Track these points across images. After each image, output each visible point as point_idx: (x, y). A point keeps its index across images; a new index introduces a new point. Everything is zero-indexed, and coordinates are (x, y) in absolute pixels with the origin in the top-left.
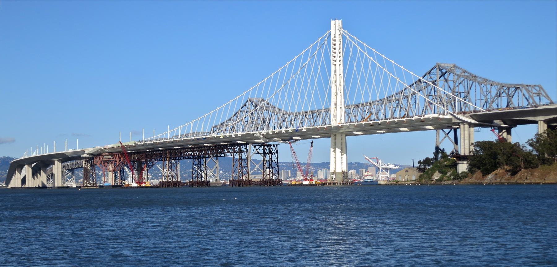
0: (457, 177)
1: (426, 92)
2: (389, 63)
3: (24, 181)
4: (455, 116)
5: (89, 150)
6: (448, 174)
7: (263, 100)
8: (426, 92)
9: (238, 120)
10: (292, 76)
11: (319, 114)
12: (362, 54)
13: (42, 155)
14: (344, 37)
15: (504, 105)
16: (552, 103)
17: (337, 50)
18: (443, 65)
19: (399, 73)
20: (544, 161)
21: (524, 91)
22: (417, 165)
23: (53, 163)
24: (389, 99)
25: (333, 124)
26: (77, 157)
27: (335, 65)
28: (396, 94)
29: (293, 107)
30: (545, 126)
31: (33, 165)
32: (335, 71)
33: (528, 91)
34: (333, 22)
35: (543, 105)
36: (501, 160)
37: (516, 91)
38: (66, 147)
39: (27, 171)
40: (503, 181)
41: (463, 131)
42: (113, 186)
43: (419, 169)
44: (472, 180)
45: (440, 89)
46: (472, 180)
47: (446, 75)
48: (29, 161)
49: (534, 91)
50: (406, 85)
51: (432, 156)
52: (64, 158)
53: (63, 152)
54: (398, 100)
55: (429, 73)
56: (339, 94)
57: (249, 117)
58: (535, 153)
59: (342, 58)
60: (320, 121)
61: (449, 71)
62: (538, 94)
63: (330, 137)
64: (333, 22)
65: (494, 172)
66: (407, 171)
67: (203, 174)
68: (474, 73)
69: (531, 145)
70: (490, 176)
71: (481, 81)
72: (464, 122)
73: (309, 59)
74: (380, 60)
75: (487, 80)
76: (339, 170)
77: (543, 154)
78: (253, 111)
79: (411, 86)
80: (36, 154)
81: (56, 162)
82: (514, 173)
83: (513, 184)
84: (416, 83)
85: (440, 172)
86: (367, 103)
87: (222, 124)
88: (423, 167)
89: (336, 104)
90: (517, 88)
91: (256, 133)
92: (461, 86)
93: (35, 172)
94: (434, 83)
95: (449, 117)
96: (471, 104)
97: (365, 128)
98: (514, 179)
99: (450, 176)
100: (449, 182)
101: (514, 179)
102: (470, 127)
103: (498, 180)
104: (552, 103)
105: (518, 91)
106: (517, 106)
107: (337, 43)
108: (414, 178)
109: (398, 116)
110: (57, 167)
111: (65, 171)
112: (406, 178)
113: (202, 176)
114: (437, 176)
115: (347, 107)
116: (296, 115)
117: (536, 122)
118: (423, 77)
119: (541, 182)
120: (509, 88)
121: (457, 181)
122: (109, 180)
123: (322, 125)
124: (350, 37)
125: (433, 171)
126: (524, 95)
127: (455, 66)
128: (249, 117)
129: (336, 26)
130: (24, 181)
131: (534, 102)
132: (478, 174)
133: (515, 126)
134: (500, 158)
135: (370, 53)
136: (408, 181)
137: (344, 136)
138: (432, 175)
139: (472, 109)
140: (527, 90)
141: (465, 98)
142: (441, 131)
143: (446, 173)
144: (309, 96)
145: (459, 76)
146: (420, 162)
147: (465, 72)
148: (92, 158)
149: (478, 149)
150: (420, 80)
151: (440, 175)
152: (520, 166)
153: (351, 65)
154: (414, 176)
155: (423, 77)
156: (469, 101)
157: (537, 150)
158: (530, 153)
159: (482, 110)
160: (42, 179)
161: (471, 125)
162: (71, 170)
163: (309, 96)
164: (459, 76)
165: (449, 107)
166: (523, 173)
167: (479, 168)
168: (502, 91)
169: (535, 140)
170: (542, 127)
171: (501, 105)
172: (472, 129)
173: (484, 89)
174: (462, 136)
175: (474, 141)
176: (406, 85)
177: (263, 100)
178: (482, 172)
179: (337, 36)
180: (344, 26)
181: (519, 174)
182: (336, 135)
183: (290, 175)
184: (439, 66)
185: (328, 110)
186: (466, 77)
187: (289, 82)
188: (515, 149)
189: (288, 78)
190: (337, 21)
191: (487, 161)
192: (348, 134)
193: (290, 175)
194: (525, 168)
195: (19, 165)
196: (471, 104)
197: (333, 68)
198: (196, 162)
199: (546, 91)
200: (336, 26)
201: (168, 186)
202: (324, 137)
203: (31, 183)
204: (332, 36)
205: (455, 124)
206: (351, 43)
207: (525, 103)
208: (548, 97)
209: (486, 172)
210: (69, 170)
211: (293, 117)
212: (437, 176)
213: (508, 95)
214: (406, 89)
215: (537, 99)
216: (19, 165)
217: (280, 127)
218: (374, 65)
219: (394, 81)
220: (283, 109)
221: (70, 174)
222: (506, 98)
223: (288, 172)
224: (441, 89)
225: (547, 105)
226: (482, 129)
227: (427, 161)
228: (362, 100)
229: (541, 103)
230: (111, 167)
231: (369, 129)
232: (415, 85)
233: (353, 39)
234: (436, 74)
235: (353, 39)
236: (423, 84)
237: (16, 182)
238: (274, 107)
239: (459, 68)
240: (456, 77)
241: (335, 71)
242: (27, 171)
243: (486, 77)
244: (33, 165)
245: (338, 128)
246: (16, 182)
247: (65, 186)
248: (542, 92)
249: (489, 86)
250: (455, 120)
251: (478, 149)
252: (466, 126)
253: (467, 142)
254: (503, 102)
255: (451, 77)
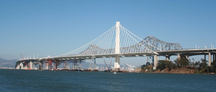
0: (153, 71)
1: (144, 44)
2: (134, 36)
3: (20, 67)
4: (152, 52)
5: (41, 59)
6: (150, 70)
7: (95, 45)
8: (144, 44)
9: (87, 51)
10: (104, 38)
11: (112, 50)
12: (125, 32)
13: (26, 59)
14: (120, 27)
15: (168, 49)
16: (182, 49)
17: (118, 31)
18: (150, 36)
19: (136, 39)
20: (179, 67)
21: (174, 45)
22: (141, 67)
23: (30, 62)
24: (133, 46)
25: (116, 54)
26: (37, 60)
27: (117, 35)
28: (135, 45)
29: (104, 47)
30: (180, 56)
31: (23, 63)
32: (117, 37)
33: (175, 45)
34: (117, 22)
35: (179, 50)
36: (166, 66)
37: (171, 45)
38: (34, 57)
39: (21, 64)
40: (166, 73)
41: (155, 57)
42: (48, 70)
43: (142, 68)
44: (156, 72)
45: (149, 44)
46: (156, 72)
47: (151, 40)
48: (22, 61)
49: (177, 45)
50: (138, 42)
51: (145, 64)
52: (33, 61)
53: (33, 59)
54: (136, 47)
55: (146, 39)
56: (118, 45)
57: (91, 50)
58: (176, 64)
59: (119, 33)
60: (112, 52)
61: (152, 39)
62: (178, 46)
63: (115, 57)
64: (117, 22)
65: (164, 70)
66: (138, 69)
67: (67, 67)
68: (159, 39)
69: (175, 62)
70: (162, 71)
71: (161, 42)
72: (155, 54)
73: (109, 33)
74: (131, 34)
75: (163, 42)
76: (117, 68)
77: (179, 65)
78: (92, 48)
79: (140, 43)
80: (25, 59)
81: (31, 62)
82: (170, 70)
83: (169, 73)
84: (141, 42)
85: (148, 69)
86: (129, 47)
87: (82, 52)
88: (142, 67)
89: (117, 47)
90: (172, 44)
91: (93, 55)
92: (155, 43)
93: (24, 65)
94: (147, 42)
95: (151, 52)
96: (158, 49)
97: (140, 54)
98: (170, 72)
99: (151, 70)
100: (150, 72)
101: (170, 72)
102: (157, 56)
103: (165, 72)
104: (182, 49)
105: (172, 45)
106: (172, 50)
107: (118, 29)
108: (140, 71)
109: (141, 51)
110: (31, 63)
111: (34, 65)
112: (138, 70)
113: (66, 68)
114: (147, 70)
115: (120, 48)
116: (105, 50)
117: (177, 55)
118: (144, 40)
119: (178, 73)
120: (169, 44)
121: (152, 72)
122: (47, 68)
123: (89, 55)
124: (122, 27)
125: (146, 68)
126: (174, 46)
127: (153, 37)
128: (91, 50)
129: (118, 24)
130: (20, 67)
131: (177, 49)
132: (159, 70)
133: (171, 56)
134: (166, 66)
135: (128, 32)
136: (138, 71)
137: (119, 57)
138: (145, 70)
139: (158, 50)
140: (175, 45)
141: (156, 47)
142: (148, 57)
143: (149, 70)
144: (109, 44)
145: (155, 40)
146: (142, 66)
147: (156, 39)
148: (42, 61)
149: (159, 62)
150: (143, 41)
151: (148, 70)
152: (172, 68)
153: (122, 35)
154: (140, 70)
155: (144, 40)
156: (157, 48)
157: (177, 63)
158: (175, 64)
159: (161, 51)
160: (26, 68)
161: (157, 55)
162: (36, 64)
163: (109, 44)
164: (155, 40)
165: (151, 49)
166: (172, 70)
167: (159, 68)
168: (167, 45)
169: (176, 60)
170: (178, 56)
171: (166, 50)
172: (158, 57)
173: (162, 44)
174: (155, 58)
175: (158, 60)
176: (138, 42)
177: (95, 45)
178: (160, 69)
179: (118, 26)
180: (120, 24)
181: (171, 70)
182: (116, 57)
183: (104, 68)
184: (149, 37)
185: (114, 49)
186: (157, 40)
187: (103, 40)
188: (170, 63)
189: (103, 39)
190: (118, 22)
191: (162, 66)
192: (121, 57)
193: (104, 68)
194: (173, 69)
195: (19, 63)
196: (158, 49)
197: (116, 36)
198: (74, 63)
199: (181, 45)
200: (118, 24)
201: (74, 71)
202: (107, 57)
203: (22, 68)
204: (117, 27)
205: (153, 55)
206: (122, 29)
207: (174, 49)
208: (181, 47)
209: (161, 70)
210: (35, 64)
211: (104, 51)
212: (147, 70)
213: (169, 46)
214: (138, 44)
215: (178, 48)
216: (19, 63)
217: (100, 54)
218: (129, 36)
219: (135, 41)
220: (101, 48)
221: (35, 65)
222: (169, 47)
223: (103, 67)
224: (149, 44)
225: (181, 50)
226: (160, 56)
227: (144, 66)
228: (125, 46)
229: (179, 49)
230: (48, 64)
231: (126, 56)
232: (141, 42)
233: (123, 28)
234: (147, 39)
235: (123, 28)
236: (144, 42)
237: (18, 68)
238: (98, 48)
239: (155, 38)
240: (154, 40)
241: (117, 37)
242: (21, 64)
243: (163, 41)
244: (23, 63)
245: (117, 55)
246: (18, 68)
247: (33, 69)
248: (179, 46)
249: (163, 43)
250: (152, 54)
251: (159, 62)
252: (156, 55)
253: (156, 60)
254: (168, 48)
255: (152, 41)
